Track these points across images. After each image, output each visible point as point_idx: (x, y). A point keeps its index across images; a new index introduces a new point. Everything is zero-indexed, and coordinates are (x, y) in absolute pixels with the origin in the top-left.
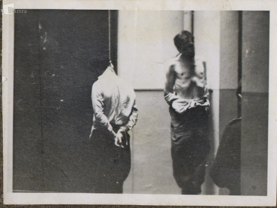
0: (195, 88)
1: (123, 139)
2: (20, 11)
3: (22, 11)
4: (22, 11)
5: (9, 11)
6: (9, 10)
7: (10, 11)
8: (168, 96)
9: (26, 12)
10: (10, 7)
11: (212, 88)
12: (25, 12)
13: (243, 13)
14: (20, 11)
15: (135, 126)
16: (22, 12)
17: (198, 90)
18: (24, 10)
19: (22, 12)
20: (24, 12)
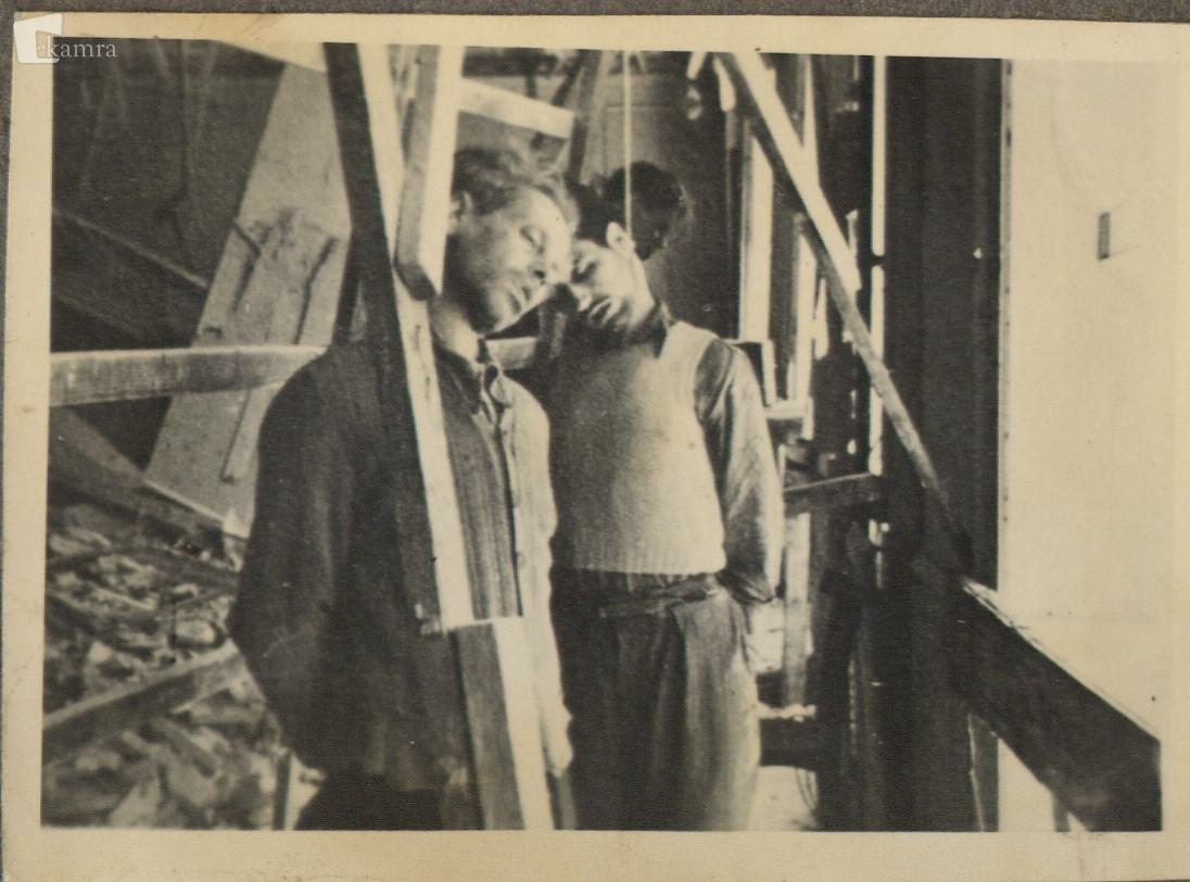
0: (981, 674)
1: (263, 338)
2: (88, 49)
3: (99, 46)
4: (95, 50)
5: (38, 51)
6: (38, 45)
7: (43, 47)
8: (93, 396)
9: (114, 55)
10: (42, 33)
11: (505, 620)
12: (110, 54)
13: (287, 75)
14: (88, 49)
15: (233, 428)
16: (95, 53)
17: (200, 90)
18: (106, 45)
19: (95, 53)
20: (104, 51)
